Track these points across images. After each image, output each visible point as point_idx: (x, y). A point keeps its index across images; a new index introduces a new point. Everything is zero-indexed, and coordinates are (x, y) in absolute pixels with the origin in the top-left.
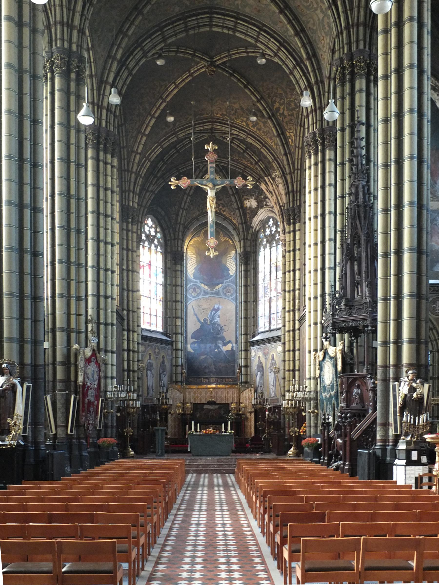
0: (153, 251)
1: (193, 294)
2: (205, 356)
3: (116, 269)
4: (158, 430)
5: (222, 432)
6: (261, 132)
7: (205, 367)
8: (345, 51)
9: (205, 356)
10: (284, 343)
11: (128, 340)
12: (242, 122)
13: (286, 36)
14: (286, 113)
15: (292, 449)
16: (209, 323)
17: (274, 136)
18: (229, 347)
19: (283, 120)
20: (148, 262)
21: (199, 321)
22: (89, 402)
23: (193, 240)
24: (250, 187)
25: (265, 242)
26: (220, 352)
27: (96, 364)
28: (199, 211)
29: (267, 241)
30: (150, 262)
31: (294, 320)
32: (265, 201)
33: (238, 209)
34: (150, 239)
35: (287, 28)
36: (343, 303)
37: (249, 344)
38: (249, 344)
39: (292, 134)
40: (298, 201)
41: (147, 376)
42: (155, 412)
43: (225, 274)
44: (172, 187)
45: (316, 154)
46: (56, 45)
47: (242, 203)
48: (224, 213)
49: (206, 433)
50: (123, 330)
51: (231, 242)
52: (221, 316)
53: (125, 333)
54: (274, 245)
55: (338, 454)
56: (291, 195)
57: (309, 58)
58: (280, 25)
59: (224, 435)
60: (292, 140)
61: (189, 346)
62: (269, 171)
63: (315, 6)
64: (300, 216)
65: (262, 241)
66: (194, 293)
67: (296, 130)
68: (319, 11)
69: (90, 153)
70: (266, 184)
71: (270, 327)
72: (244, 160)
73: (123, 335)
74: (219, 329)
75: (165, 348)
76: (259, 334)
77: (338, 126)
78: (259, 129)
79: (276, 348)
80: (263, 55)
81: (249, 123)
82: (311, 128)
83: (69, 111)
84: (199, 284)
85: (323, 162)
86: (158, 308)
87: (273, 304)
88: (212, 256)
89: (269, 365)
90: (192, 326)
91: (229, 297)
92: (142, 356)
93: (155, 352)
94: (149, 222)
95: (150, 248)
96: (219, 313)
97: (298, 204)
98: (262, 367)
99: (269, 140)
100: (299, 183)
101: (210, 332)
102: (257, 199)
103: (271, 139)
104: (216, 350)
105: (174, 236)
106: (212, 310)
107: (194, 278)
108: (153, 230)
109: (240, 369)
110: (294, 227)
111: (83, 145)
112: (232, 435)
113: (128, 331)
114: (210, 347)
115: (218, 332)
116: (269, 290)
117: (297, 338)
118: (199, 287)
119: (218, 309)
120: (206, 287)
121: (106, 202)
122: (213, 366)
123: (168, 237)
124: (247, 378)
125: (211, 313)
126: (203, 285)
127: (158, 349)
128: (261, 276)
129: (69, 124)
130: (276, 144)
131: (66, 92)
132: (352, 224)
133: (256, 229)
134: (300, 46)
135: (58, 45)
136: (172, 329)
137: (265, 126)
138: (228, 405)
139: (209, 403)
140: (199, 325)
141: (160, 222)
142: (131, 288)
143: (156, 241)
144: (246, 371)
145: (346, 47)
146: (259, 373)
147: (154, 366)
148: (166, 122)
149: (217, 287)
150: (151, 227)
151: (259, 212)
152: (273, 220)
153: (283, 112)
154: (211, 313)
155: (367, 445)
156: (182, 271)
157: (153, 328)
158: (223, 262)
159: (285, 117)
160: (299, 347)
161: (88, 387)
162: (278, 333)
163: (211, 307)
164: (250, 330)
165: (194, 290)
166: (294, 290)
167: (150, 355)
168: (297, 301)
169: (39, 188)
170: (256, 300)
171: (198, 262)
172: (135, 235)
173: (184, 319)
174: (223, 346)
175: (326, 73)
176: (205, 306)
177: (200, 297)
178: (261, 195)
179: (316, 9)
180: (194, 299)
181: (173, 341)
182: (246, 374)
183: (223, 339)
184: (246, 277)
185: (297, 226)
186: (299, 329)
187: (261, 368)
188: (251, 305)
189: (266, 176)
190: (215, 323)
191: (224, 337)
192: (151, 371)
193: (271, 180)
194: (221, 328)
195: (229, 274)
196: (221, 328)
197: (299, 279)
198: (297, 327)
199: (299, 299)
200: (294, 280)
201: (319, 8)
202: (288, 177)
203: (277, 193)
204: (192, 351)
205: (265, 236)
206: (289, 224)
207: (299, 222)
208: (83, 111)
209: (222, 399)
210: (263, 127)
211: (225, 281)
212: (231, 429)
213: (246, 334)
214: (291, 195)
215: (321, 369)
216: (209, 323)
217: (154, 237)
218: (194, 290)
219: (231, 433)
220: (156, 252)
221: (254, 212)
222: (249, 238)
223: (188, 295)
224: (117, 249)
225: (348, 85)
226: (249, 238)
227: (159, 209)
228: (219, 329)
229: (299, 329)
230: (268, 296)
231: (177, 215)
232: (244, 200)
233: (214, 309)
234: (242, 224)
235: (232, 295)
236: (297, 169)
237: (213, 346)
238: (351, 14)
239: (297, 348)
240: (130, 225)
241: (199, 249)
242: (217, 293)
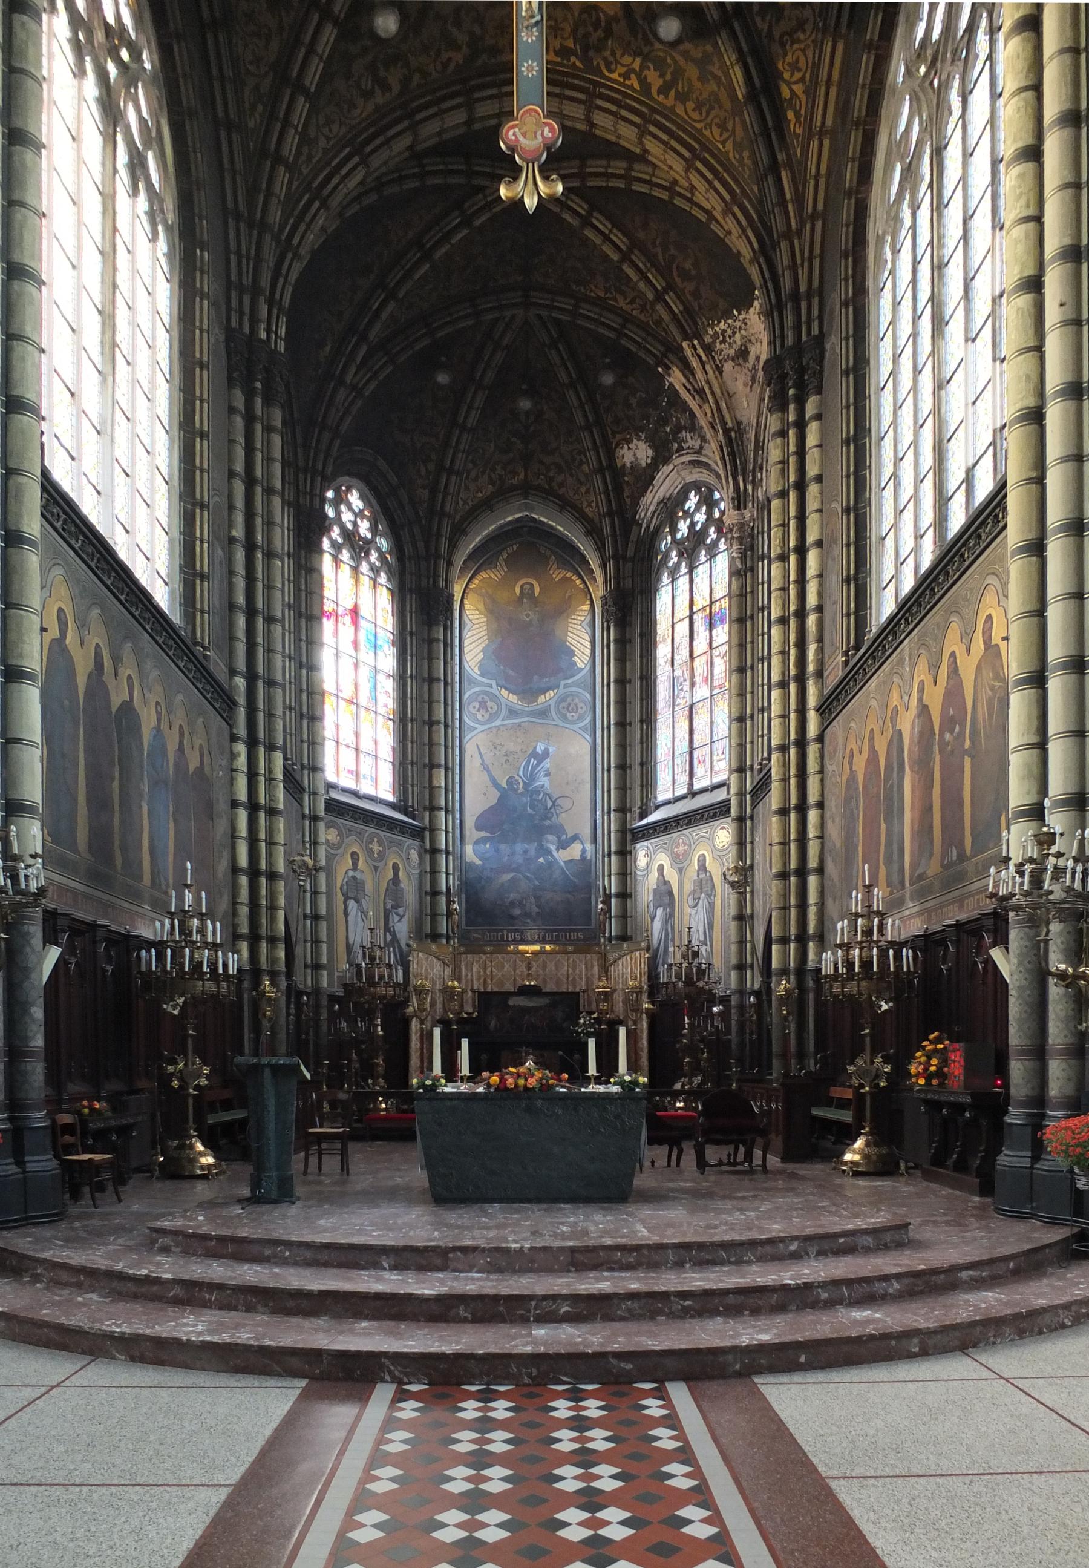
0: (365, 581)
1: (479, 716)
2: (512, 875)
4: (257, 1069)
5: (587, 1080)
6: (690, 105)
7: (512, 903)
9: (512, 875)
11: (252, 775)
12: (626, 76)
15: (859, 1144)
16: (521, 790)
18: (575, 851)
19: (770, 36)
20: (350, 606)
21: (495, 784)
23: (479, 577)
26: (551, 864)
28: (493, 483)
29: (680, 555)
30: (356, 606)
31: (802, 711)
32: (675, 439)
33: (601, 470)
37: (629, 837)
38: (629, 837)
40: (815, 326)
41: (346, 914)
42: (369, 1015)
43: (564, 665)
47: (611, 455)
48: (562, 491)
49: (502, 1088)
50: (234, 738)
51: (578, 582)
52: (553, 771)
53: (241, 748)
54: (703, 559)
59: (594, 1096)
60: (797, 116)
61: (469, 849)
62: (696, 324)
64: (821, 372)
65: (666, 556)
66: (482, 712)
67: (816, 67)
70: (687, 369)
71: (691, 784)
72: (620, 299)
73: (233, 756)
74: (549, 804)
75: (400, 844)
76: (657, 807)
78: (682, 98)
79: (711, 839)
84: (495, 690)
86: (382, 738)
87: (701, 720)
88: (530, 203)
89: (689, 886)
90: (477, 795)
91: (573, 723)
92: (330, 858)
93: (370, 852)
94: (355, 500)
95: (355, 570)
96: (547, 764)
97: (815, 331)
98: (670, 893)
99: (716, 132)
100: (816, 263)
101: (523, 814)
102: (651, 441)
103: (723, 127)
104: (541, 860)
105: (427, 547)
106: (530, 757)
107: (482, 675)
109: (607, 901)
110: (801, 411)
112: (636, 1099)
113: (252, 743)
114: (525, 852)
115: (547, 814)
116: (687, 686)
117: (812, 765)
118: (494, 698)
119: (546, 754)
120: (513, 698)
122: (533, 900)
123: (408, 549)
124: (624, 927)
125: (528, 763)
126: (504, 693)
127: (380, 843)
128: (663, 651)
133: (648, 527)
136: (421, 795)
137: (703, 79)
138: (575, 996)
139: (524, 991)
140: (494, 796)
141: (387, 509)
143: (374, 556)
144: (624, 908)
146: (660, 911)
147: (369, 887)
149: (542, 699)
150: (359, 514)
151: (660, 477)
152: (698, 491)
154: (528, 763)
156: (448, 645)
157: (366, 788)
158: (558, 633)
160: (822, 795)
162: (721, 795)
163: (527, 744)
164: (635, 797)
165: (483, 705)
166: (801, 614)
167: (355, 857)
168: (812, 649)
170: (649, 719)
171: (492, 634)
173: (454, 770)
174: (558, 849)
176: (511, 746)
177: (498, 723)
178: (666, 424)
180: (481, 728)
181: (424, 829)
182: (624, 916)
183: (558, 830)
184: (622, 660)
185: (811, 407)
186: (752, 818)
187: (665, 895)
188: (635, 733)
189: (686, 337)
190: (537, 791)
191: (562, 826)
192: (357, 901)
193: (700, 351)
194: (554, 802)
195: (575, 664)
196: (554, 802)
197: (820, 576)
198: (812, 730)
199: (820, 640)
200: (802, 581)
203: (717, 391)
204: (478, 862)
207: (819, 391)
209: (558, 982)
210: (697, 85)
211: (562, 683)
212: (633, 1067)
213: (622, 810)
216: (521, 790)
217: (368, 542)
218: (483, 705)
219: (634, 1083)
220: (375, 584)
221: (645, 478)
222: (630, 552)
223: (466, 718)
226: (630, 552)
227: (382, 464)
228: (549, 804)
229: (820, 739)
230: (683, 702)
231: (434, 491)
232: (617, 445)
233: (534, 754)
234: (610, 514)
235: (581, 718)
236: (813, 217)
237: (532, 848)
239: (813, 797)
240: (259, 401)
241: (494, 601)
242: (544, 713)
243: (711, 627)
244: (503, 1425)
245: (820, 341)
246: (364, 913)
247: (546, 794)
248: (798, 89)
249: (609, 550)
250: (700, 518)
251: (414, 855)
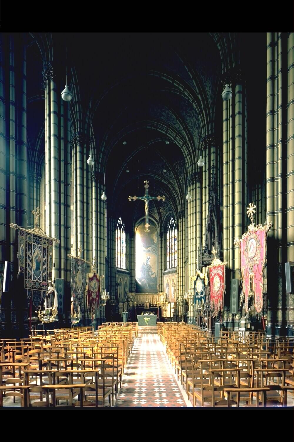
0: (122, 232)
3: (106, 239)
8: (207, 134)
10: (178, 274)
13: (179, 130)
14: (179, 168)
17: (174, 179)
22: (93, 299)
24: (164, 200)
25: (169, 228)
27: (97, 280)
29: (171, 227)
34: (120, 226)
35: (180, 126)
36: (207, 252)
39: (181, 178)
44: (130, 200)
45: (193, 185)
46: (77, 131)
54: (173, 229)
55: (205, 325)
56: (181, 205)
57: (189, 140)
58: (177, 125)
63: (192, 115)
65: (169, 227)
68: (194, 118)
69: (94, 184)
77: (204, 170)
78: (167, 176)
80: (168, 140)
81: (163, 173)
82: (190, 172)
83: (83, 161)
85: (196, 188)
94: (120, 219)
103: (172, 180)
108: (121, 223)
111: (90, 178)
119: (149, 258)
121: (100, 207)
124: (162, 290)
129: (84, 168)
130: (174, 183)
131: (82, 153)
132: (210, 215)
134: (185, 134)
135: (78, 131)
137: (170, 174)
142: (112, 248)
145: (194, 170)
148: (123, 144)
150: (121, 221)
153: (177, 168)
155: (219, 320)
156: (134, 241)
159: (178, 170)
161: (92, 291)
169: (68, 195)
172: (114, 224)
175: (197, 147)
179: (193, 117)
183: (152, 272)
186: (185, 267)
201: (194, 117)
202: (180, 197)
205: (170, 224)
206: (193, 184)
208: (90, 159)
214: (181, 205)
215: (195, 284)
217: (122, 225)
224: (106, 229)
225: (194, 185)
226: (163, 226)
238: (209, 116)
243: (175, 241)
244: (144, 398)
245: (184, 211)
246: (122, 288)
247: (150, 265)
248: (181, 178)
249: (159, 225)
250: (173, 222)
251: (129, 277)
